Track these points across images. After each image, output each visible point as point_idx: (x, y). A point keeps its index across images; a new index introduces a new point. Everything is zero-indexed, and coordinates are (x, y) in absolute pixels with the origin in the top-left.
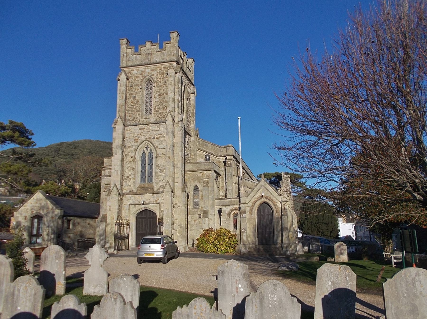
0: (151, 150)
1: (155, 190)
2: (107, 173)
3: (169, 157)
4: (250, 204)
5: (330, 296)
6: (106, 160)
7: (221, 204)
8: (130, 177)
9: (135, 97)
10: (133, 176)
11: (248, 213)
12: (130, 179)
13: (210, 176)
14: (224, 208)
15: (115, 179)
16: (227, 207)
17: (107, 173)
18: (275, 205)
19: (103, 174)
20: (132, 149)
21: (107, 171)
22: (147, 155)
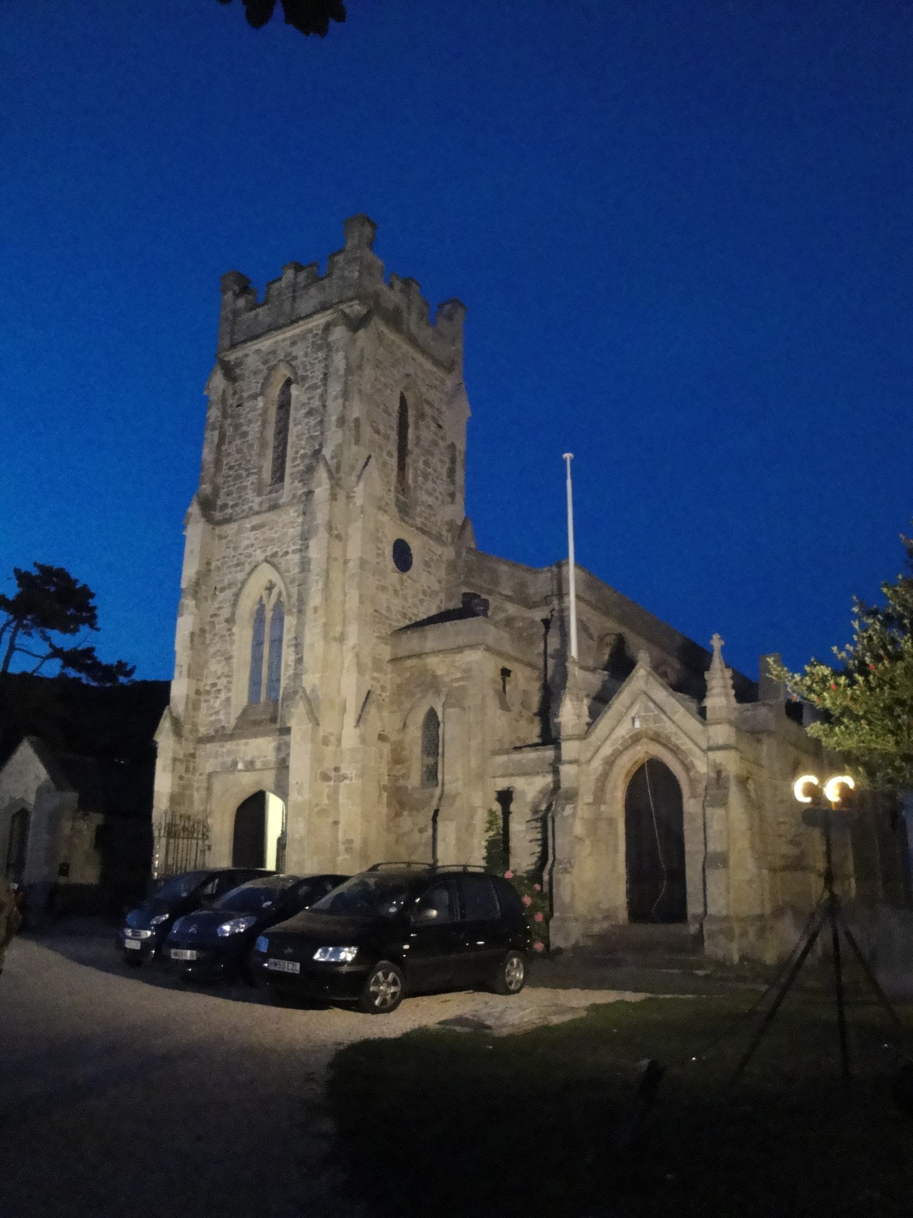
0: (280, 594)
9: (245, 434)
14: (519, 784)
16: (530, 779)
18: (688, 768)
20: (229, 593)
22: (269, 615)
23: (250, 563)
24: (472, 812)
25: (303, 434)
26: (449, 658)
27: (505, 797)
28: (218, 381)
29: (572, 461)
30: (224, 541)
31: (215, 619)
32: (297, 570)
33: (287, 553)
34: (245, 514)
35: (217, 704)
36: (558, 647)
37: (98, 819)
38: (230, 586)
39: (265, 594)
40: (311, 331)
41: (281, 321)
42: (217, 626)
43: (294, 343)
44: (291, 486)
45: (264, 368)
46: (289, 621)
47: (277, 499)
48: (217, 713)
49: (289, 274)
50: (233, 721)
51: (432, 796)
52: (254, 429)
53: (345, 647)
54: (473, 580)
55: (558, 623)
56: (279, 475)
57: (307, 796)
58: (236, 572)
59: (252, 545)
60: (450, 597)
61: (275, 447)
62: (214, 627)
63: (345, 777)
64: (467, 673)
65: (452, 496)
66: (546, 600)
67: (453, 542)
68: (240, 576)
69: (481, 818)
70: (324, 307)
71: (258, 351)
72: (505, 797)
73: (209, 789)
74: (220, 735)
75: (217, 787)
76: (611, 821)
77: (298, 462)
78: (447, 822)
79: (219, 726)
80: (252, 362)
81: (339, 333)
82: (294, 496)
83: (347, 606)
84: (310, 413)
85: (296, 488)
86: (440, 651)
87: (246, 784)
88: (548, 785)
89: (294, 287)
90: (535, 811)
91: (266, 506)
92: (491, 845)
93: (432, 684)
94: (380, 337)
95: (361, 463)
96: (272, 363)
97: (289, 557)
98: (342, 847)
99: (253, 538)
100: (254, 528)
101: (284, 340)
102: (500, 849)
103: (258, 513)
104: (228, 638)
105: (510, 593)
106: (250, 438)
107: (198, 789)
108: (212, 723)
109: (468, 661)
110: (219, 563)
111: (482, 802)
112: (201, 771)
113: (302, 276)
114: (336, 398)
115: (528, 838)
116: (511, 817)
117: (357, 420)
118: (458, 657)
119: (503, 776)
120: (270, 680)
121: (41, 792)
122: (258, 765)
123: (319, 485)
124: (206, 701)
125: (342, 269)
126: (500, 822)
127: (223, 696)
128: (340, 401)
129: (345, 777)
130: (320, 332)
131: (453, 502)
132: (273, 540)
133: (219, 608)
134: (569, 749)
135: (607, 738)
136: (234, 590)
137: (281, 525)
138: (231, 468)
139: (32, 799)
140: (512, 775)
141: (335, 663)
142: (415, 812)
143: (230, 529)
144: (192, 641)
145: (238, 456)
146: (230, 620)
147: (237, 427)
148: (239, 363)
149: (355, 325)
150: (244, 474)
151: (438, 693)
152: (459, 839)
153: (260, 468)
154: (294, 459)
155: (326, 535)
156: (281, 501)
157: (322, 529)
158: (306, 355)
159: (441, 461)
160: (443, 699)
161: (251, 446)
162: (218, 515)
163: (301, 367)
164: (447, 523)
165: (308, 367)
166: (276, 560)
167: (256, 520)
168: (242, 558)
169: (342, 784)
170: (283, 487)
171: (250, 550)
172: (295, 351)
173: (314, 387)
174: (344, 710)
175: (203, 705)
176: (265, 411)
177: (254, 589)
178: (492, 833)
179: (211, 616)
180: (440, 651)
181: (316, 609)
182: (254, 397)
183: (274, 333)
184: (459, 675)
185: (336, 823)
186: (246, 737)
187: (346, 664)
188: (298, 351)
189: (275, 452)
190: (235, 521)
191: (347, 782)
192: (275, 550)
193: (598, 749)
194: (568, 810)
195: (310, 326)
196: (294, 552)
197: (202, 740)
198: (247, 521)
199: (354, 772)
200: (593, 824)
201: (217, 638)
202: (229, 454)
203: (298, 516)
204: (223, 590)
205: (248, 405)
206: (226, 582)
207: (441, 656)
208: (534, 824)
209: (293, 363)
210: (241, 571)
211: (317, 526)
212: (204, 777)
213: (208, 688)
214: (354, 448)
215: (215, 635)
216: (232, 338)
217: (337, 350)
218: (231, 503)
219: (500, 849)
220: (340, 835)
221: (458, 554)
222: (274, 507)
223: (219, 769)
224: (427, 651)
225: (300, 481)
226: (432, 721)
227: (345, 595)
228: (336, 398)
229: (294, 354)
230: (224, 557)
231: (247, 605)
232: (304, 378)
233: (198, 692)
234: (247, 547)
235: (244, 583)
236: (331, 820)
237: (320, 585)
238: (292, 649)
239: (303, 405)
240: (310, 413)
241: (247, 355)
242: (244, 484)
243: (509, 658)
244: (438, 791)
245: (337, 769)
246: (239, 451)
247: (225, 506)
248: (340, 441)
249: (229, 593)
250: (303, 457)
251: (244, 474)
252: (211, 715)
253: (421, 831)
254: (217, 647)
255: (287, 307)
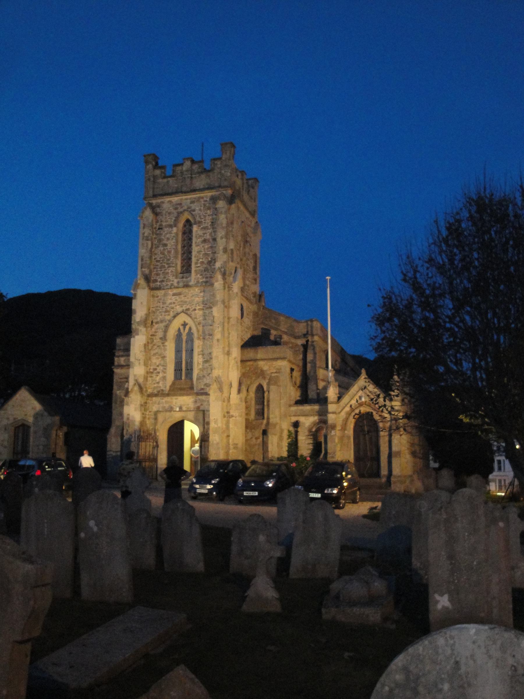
0: (190, 329)
1: (272, 338)
2: (122, 361)
3: (218, 340)
4: (343, 414)
5: (213, 464)
6: (119, 341)
7: (298, 413)
8: (158, 370)
9: (166, 245)
10: (162, 368)
11: (339, 428)
12: (159, 373)
13: (281, 369)
14: (302, 419)
15: (137, 371)
16: (307, 418)
17: (122, 361)
19: (116, 363)
20: (162, 325)
21: (122, 359)
22: (184, 337)
23: (173, 312)
24: (282, 431)
25: (201, 251)
26: (269, 363)
27: (296, 425)
28: (148, 213)
29: (330, 280)
30: (156, 299)
31: (154, 337)
32: (201, 318)
33: (195, 310)
34: (169, 287)
35: (158, 379)
36: (312, 359)
37: (65, 429)
38: (162, 321)
39: (182, 328)
40: (202, 198)
41: (184, 189)
42: (155, 341)
43: (192, 202)
44: (194, 277)
45: (175, 212)
46: (197, 344)
47: (188, 282)
48: (158, 383)
49: (188, 163)
50: (168, 388)
51: (262, 423)
52: (171, 244)
53: (230, 358)
54: (266, 323)
55: (312, 348)
56: (187, 269)
57: (220, 425)
58: (165, 315)
59: (174, 303)
60: (255, 329)
61: (183, 254)
62: (153, 341)
63: (232, 416)
64: (279, 371)
65: (255, 280)
66: (305, 335)
67: (256, 303)
68: (168, 318)
69: (285, 434)
70: (210, 188)
71: (170, 202)
72: (296, 425)
73: (156, 419)
74: (160, 394)
75: (160, 417)
76: (349, 437)
77: (199, 265)
78: (274, 436)
79: (159, 389)
80: (166, 206)
81: (221, 204)
82: (198, 282)
83: (231, 338)
84: (205, 241)
85: (198, 278)
86: (265, 359)
87: (177, 416)
88: (316, 420)
89: (191, 171)
90: (310, 431)
91: (181, 284)
92: (290, 445)
93: (262, 374)
94: (238, 208)
95: (233, 271)
96: (180, 210)
97: (197, 311)
98: (231, 447)
99: (174, 300)
100: (174, 295)
101: (186, 199)
102: (294, 445)
103: (177, 288)
104: (163, 348)
105: (286, 331)
106: (168, 247)
107: (149, 419)
108: (154, 388)
109: (279, 365)
110: (154, 309)
111: (286, 426)
112: (150, 410)
113: (196, 167)
114: (222, 238)
115: (307, 443)
116: (298, 433)
117: (232, 250)
118: (274, 363)
119: (295, 416)
120: (187, 369)
121: (37, 416)
122: (184, 408)
123: (217, 281)
124: (151, 377)
125: (220, 169)
126: (294, 435)
127: (161, 375)
128: (224, 240)
129: (232, 416)
130: (208, 200)
131: (256, 283)
132: (186, 302)
133: (156, 332)
134: (331, 407)
135: (347, 404)
136: (164, 324)
137: (190, 295)
138: (157, 261)
139: (31, 420)
140: (299, 416)
141: (223, 363)
142: (253, 430)
143: (160, 293)
144: (145, 348)
145: (162, 256)
146: (164, 339)
147: (160, 240)
148: (159, 206)
149: (231, 200)
150: (166, 266)
151: (264, 378)
152: (278, 443)
153: (176, 264)
154: (196, 263)
155: (222, 306)
156: (191, 284)
157: (219, 303)
158: (200, 210)
159: (251, 263)
160: (267, 381)
161: (169, 252)
162: (152, 285)
163: (198, 216)
164: (253, 293)
165: (202, 217)
166: (189, 312)
167: (175, 291)
168: (168, 309)
169: (231, 419)
170: (190, 276)
171: (173, 305)
172: (193, 206)
173: (205, 228)
174: (231, 386)
175: (149, 379)
176: (177, 234)
177: (176, 324)
178: (290, 440)
179: (151, 335)
180: (265, 359)
181: (218, 340)
182: (171, 226)
183: (180, 194)
184: (275, 371)
185: (228, 436)
186: (176, 395)
187: (231, 366)
188: (196, 207)
189: (182, 257)
190: (164, 289)
191: (234, 418)
192: (188, 307)
193: (344, 408)
194: (333, 433)
195: (202, 195)
196: (199, 309)
197: (151, 395)
198: (170, 290)
199: (237, 414)
200: (341, 438)
201: (156, 347)
202: (156, 254)
203: (201, 292)
204: (157, 323)
205: (166, 230)
206: (159, 319)
207: (266, 361)
208: (309, 437)
209: (193, 213)
210: (169, 315)
211: (217, 301)
212: (152, 413)
213: (151, 370)
214: (231, 263)
215: (154, 345)
216: (153, 192)
217: (221, 213)
218: (159, 280)
219: (294, 445)
220: (231, 441)
221: (259, 309)
222: (187, 286)
223: (160, 410)
224: (258, 358)
225: (201, 275)
226: (260, 389)
227: (229, 334)
228: (222, 238)
229: (193, 208)
230: (157, 307)
231: (172, 333)
232: (200, 222)
233: (147, 373)
234: (171, 304)
235: (170, 321)
236: (226, 435)
237: (220, 329)
238: (201, 356)
239: (201, 236)
240: (205, 241)
241: (163, 202)
242: (167, 271)
243: (293, 363)
244: (265, 421)
245: (228, 413)
246: (162, 253)
247: (156, 281)
248: (225, 260)
249: (162, 325)
250: (202, 263)
251: (166, 266)
252: (154, 384)
253: (257, 438)
254: (156, 351)
255: (188, 181)
